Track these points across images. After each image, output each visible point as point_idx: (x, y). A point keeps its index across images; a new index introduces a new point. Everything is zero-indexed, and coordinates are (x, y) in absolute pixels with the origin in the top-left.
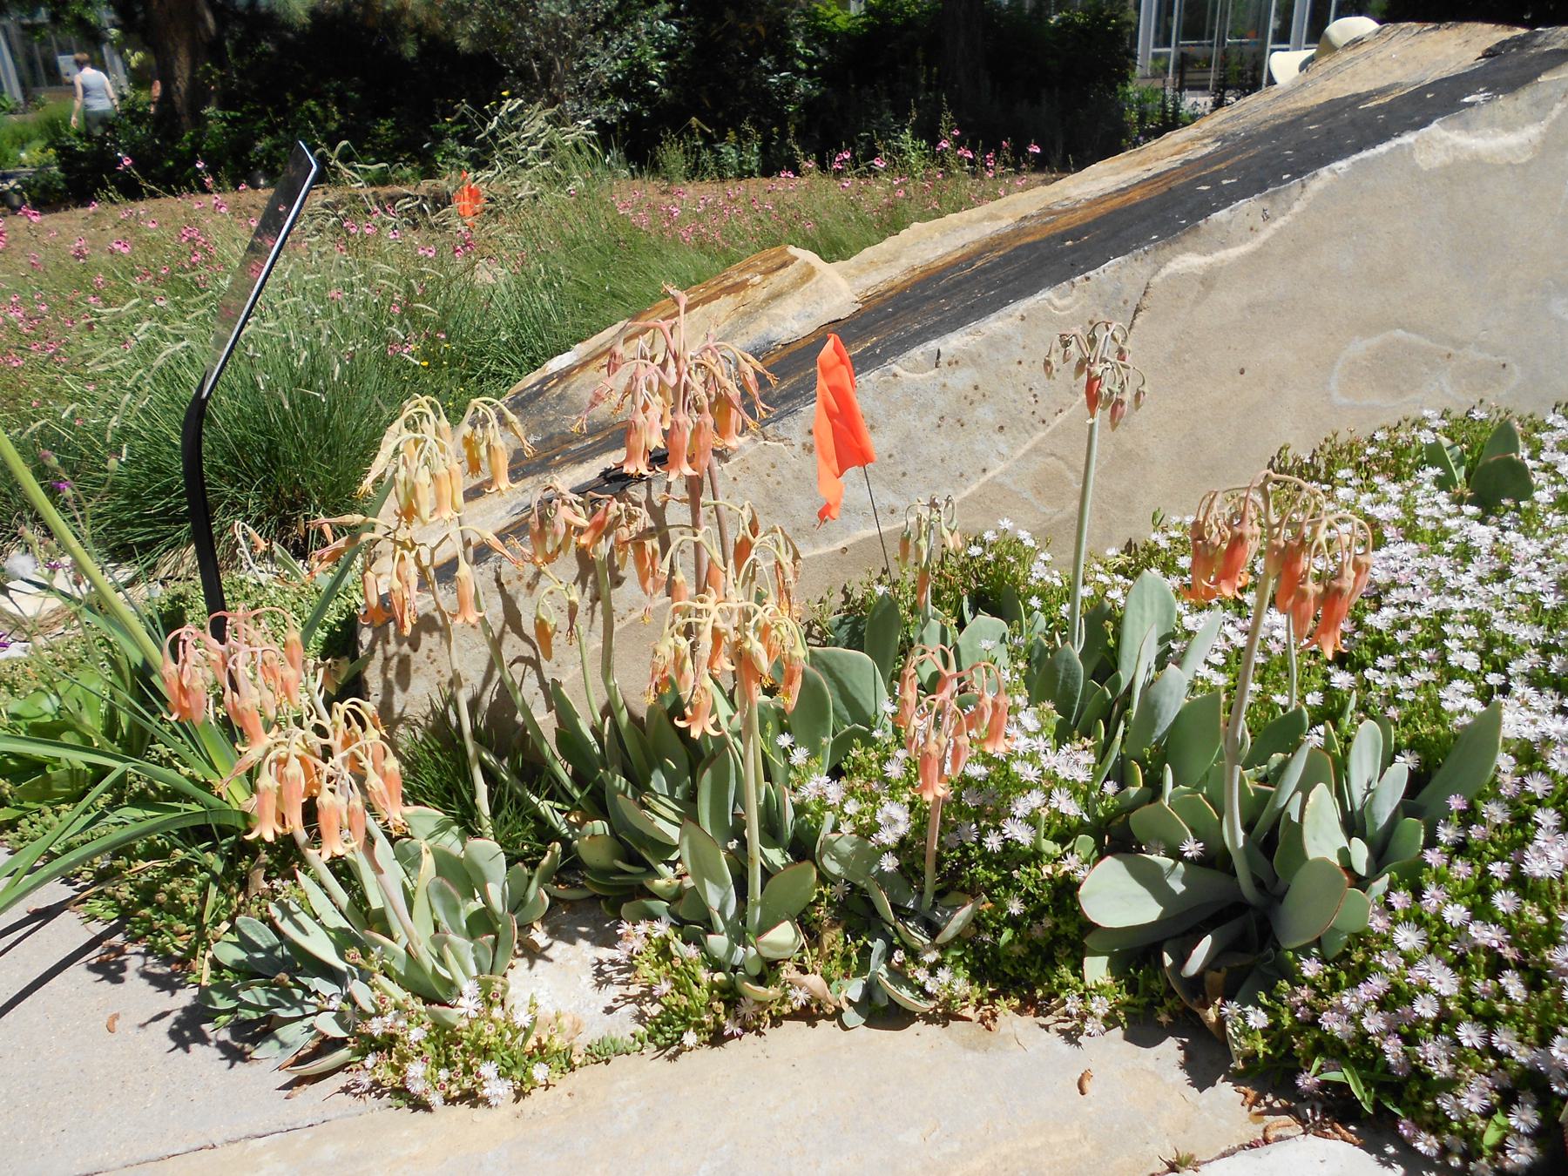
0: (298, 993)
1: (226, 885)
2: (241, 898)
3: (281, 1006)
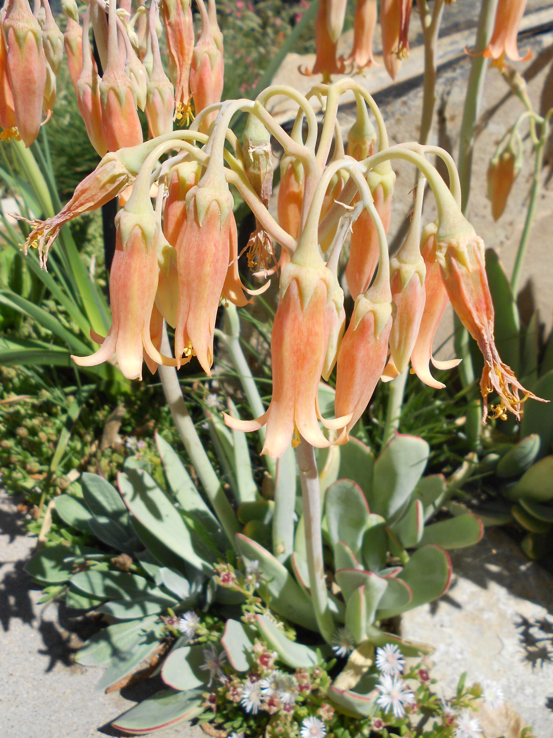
0: (141, 582)
1: (82, 431)
2: (93, 448)
3: (118, 599)
